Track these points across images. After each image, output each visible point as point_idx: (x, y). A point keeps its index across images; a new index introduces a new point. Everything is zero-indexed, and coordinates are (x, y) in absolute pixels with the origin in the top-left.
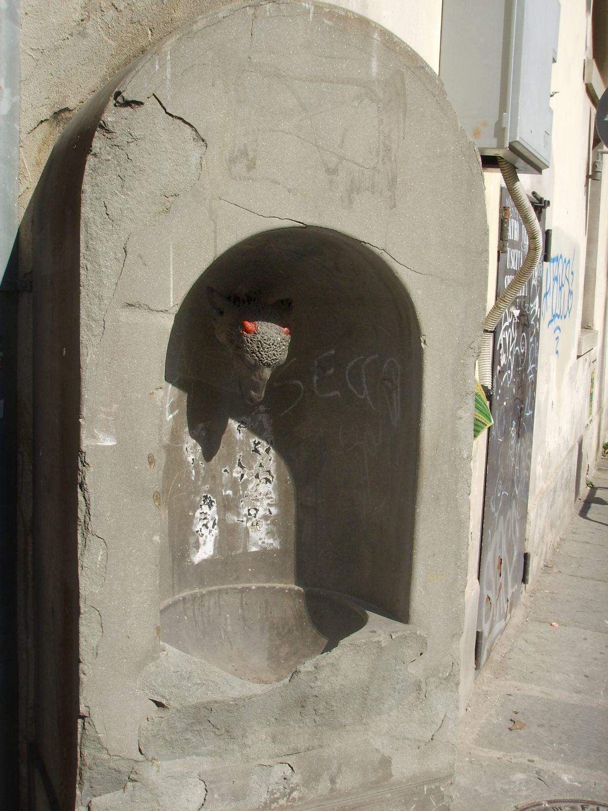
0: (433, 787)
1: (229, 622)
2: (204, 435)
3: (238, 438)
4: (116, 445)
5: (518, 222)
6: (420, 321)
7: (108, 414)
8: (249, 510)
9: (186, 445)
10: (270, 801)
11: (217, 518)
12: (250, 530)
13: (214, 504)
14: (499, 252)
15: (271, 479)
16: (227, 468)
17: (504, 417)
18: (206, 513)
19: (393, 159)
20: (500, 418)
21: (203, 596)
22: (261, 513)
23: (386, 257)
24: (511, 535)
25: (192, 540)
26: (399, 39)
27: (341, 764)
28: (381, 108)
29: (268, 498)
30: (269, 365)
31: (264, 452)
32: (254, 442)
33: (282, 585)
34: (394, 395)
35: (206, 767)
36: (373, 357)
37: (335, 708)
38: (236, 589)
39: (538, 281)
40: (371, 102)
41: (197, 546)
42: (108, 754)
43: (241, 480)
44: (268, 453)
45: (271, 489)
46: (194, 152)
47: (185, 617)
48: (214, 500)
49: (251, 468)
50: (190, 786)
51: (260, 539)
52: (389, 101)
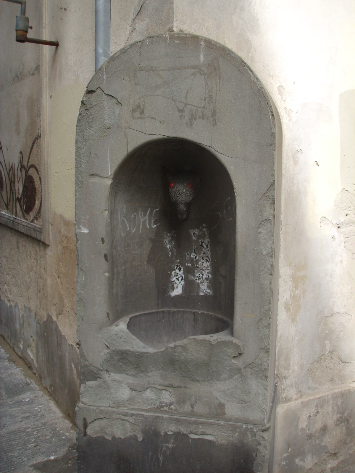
3: (193, 239)
4: (88, 233)
6: (233, 181)
7: (85, 219)
8: (199, 274)
9: (165, 240)
10: (160, 407)
11: (183, 276)
12: (200, 284)
15: (209, 260)
16: (188, 253)
18: (178, 273)
19: (214, 101)
21: (174, 312)
22: (205, 276)
23: (212, 150)
25: (170, 285)
29: (208, 270)
30: (182, 203)
31: (205, 246)
32: (201, 241)
33: (212, 313)
35: (131, 381)
37: (191, 370)
38: (192, 312)
40: (201, 75)
41: (173, 288)
43: (195, 259)
44: (207, 247)
45: (209, 265)
47: (164, 320)
48: (182, 267)
49: (200, 254)
50: (123, 388)
51: (205, 289)
52: (211, 73)
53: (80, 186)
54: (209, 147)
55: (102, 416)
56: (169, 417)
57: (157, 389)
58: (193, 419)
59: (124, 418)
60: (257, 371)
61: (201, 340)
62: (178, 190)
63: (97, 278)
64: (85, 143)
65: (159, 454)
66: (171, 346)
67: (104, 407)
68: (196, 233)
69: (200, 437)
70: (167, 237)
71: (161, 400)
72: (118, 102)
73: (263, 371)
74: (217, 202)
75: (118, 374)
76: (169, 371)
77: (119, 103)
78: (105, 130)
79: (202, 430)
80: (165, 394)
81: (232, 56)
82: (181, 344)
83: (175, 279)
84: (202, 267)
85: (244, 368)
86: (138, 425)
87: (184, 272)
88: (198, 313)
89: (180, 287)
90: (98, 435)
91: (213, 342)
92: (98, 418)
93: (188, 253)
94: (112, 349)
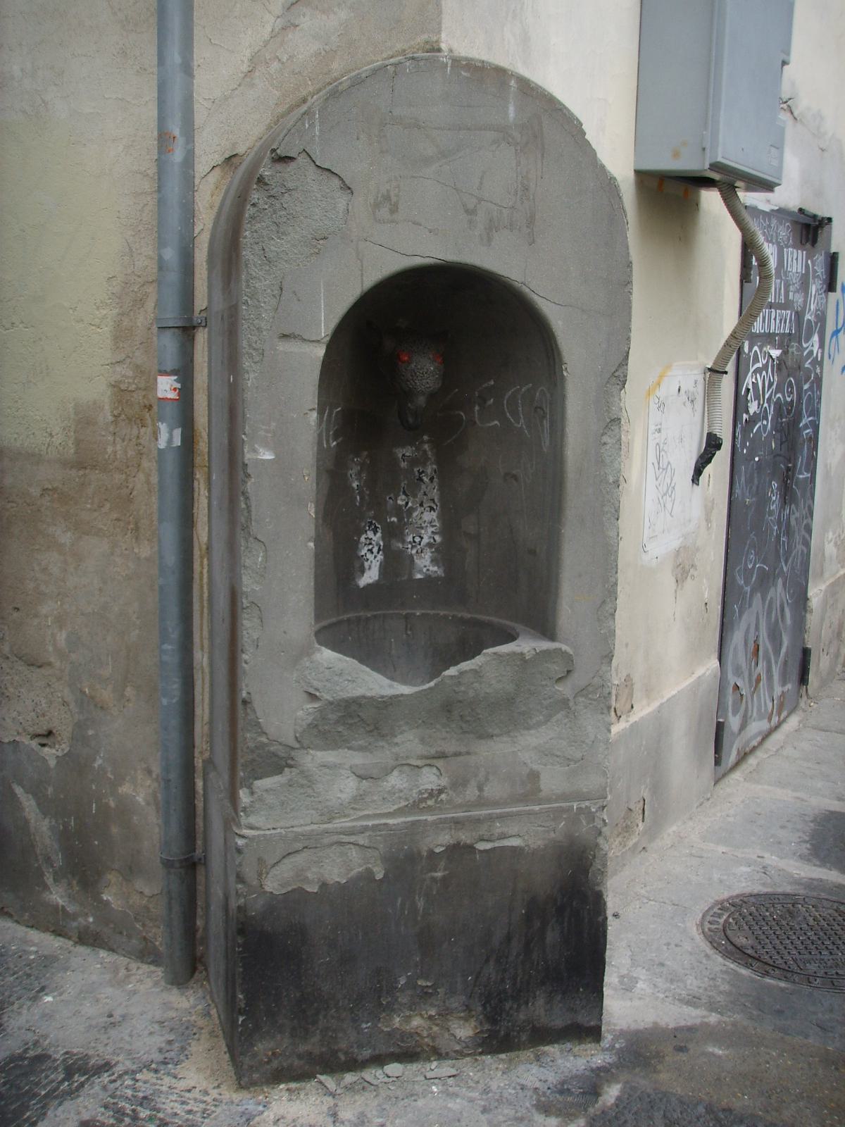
0: (583, 806)
1: (393, 646)
2: (368, 462)
5: (775, 246)
8: (414, 537)
11: (382, 543)
12: (415, 557)
13: (380, 531)
14: (741, 282)
15: (435, 507)
17: (756, 475)
18: (371, 539)
19: (531, 198)
20: (748, 476)
21: (368, 619)
22: (426, 540)
24: (777, 620)
25: (357, 565)
26: (536, 84)
27: (488, 773)
28: (519, 151)
29: (433, 526)
32: (419, 471)
33: (446, 612)
34: (545, 421)
36: (527, 386)
37: (481, 716)
39: (817, 316)
41: (362, 571)
42: (268, 739)
43: (406, 507)
44: (432, 482)
45: (434, 517)
46: (342, 201)
48: (379, 526)
49: (415, 496)
51: (425, 566)
53: (257, 359)
54: (520, 285)
55: (299, 846)
56: (438, 819)
57: (413, 767)
58: (484, 812)
59: (345, 839)
60: (595, 700)
61: (508, 655)
62: (419, 367)
63: (290, 554)
64: (268, 268)
65: (417, 898)
66: (453, 674)
67: (302, 825)
68: (407, 454)
69: (497, 844)
70: (354, 465)
71: (420, 789)
72: (345, 185)
73: (605, 698)
74: (457, 390)
75: (330, 752)
76: (438, 726)
77: (347, 188)
78: (314, 242)
79: (498, 831)
80: (428, 775)
81: (565, 115)
82: (473, 667)
83: (366, 552)
84: (419, 522)
85: (574, 697)
86: (374, 848)
87: (382, 536)
88: (414, 614)
89: (376, 566)
90: (290, 889)
91: (527, 654)
92: (290, 851)
93: (392, 495)
94: (327, 700)
